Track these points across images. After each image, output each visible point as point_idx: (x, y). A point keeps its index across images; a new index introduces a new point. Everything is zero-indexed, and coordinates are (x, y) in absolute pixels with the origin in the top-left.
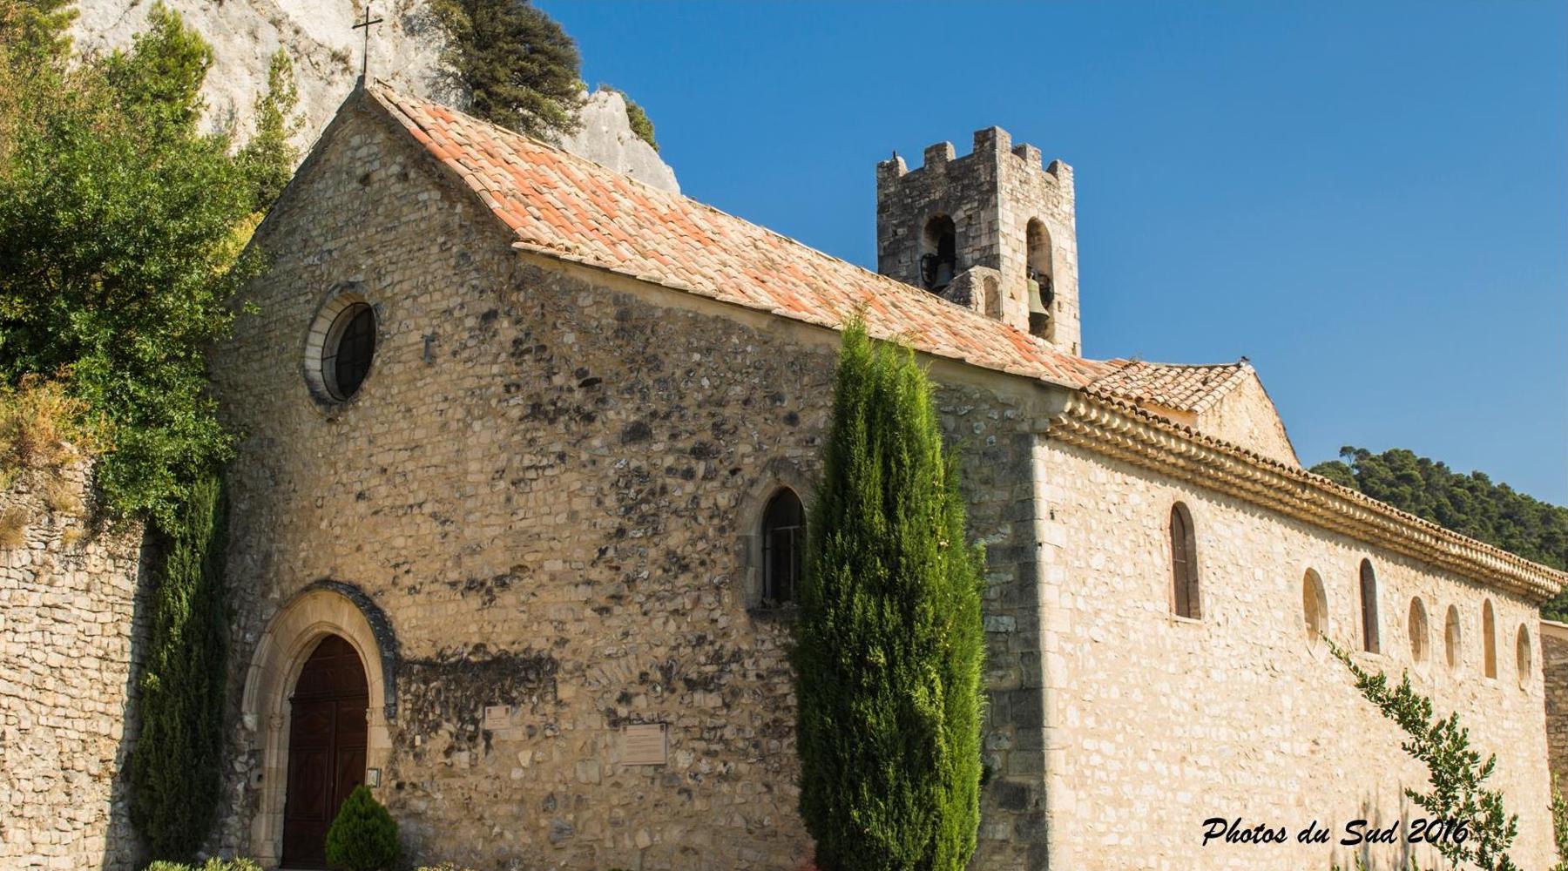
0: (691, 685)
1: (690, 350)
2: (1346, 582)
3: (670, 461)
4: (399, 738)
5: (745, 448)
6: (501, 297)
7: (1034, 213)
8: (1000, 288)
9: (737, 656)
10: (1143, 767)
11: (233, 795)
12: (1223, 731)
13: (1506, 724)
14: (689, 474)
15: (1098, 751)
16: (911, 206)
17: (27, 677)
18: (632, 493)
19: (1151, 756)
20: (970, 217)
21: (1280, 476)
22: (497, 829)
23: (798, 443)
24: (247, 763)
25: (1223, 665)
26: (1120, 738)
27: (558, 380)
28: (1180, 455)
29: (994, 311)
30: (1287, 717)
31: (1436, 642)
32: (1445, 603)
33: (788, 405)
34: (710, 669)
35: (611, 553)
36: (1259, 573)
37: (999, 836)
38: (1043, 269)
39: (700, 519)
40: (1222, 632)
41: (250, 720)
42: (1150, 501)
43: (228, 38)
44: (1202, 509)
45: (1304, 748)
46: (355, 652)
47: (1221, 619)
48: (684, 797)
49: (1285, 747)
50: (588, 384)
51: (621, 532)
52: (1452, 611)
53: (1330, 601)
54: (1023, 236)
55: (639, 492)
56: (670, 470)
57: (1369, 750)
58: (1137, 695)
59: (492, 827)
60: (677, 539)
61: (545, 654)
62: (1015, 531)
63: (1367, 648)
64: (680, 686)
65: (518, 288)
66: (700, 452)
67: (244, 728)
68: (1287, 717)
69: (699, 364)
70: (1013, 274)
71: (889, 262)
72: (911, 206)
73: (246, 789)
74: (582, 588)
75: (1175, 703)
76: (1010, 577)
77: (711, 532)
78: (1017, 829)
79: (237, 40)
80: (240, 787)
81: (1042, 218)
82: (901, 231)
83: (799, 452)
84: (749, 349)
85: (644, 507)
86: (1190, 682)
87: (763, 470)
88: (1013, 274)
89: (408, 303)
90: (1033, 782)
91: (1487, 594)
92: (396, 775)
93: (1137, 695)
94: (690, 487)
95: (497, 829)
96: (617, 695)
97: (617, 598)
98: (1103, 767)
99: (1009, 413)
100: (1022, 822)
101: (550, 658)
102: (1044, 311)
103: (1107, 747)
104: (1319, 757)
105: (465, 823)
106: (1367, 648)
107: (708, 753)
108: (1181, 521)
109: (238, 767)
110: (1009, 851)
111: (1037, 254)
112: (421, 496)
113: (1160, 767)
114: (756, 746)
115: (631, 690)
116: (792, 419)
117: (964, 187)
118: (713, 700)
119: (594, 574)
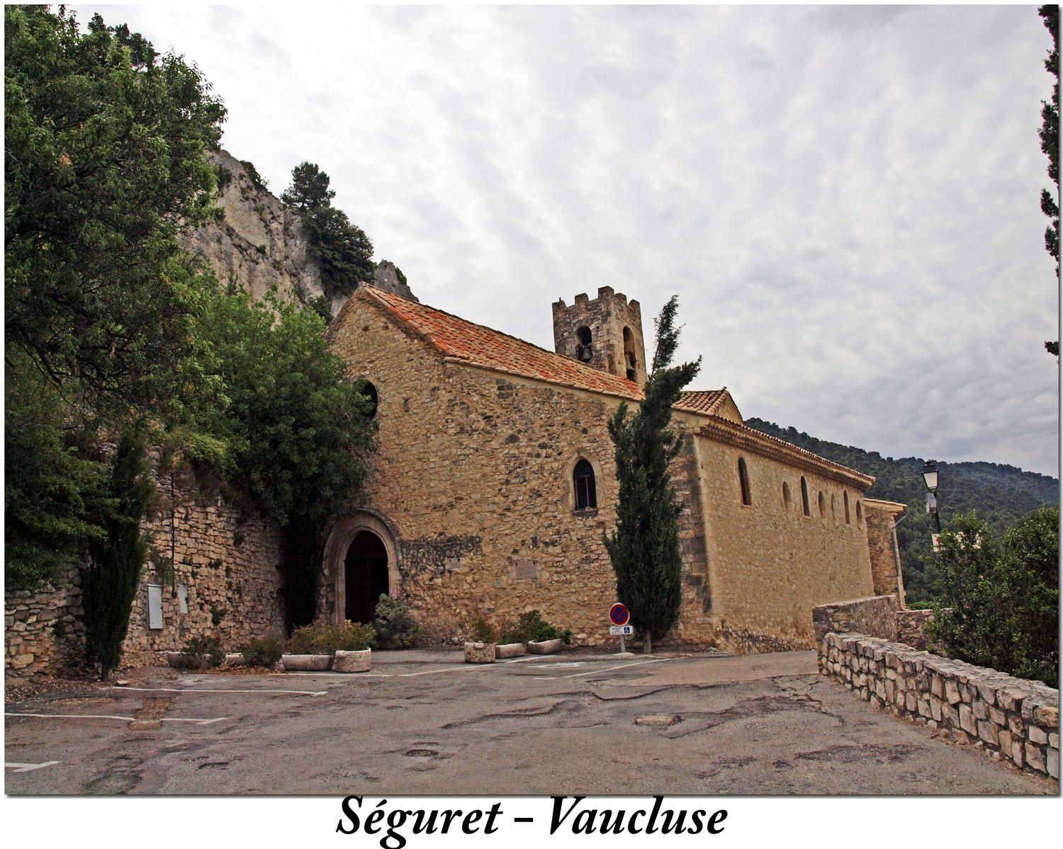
0: (547, 544)
1: (535, 402)
2: (797, 487)
3: (529, 450)
4: (405, 575)
5: (564, 444)
6: (440, 380)
7: (625, 324)
8: (614, 359)
9: (567, 531)
10: (738, 567)
11: (321, 605)
12: (762, 551)
13: (855, 543)
14: (538, 456)
15: (724, 561)
16: (570, 323)
17: (245, 557)
18: (512, 465)
19: (740, 562)
20: (598, 327)
21: (776, 445)
22: (458, 611)
23: (588, 441)
24: (326, 590)
25: (760, 524)
26: (730, 555)
27: (473, 416)
28: (743, 439)
29: (612, 371)
30: (782, 544)
31: (828, 510)
32: (830, 493)
33: (582, 425)
34: (555, 537)
35: (503, 491)
36: (768, 485)
37: (690, 597)
38: (630, 349)
39: (545, 474)
40: (758, 510)
41: (326, 572)
42: (731, 456)
43: (208, 244)
44: (749, 459)
45: (788, 557)
46: (379, 539)
47: (757, 505)
48: (546, 591)
49: (782, 556)
50: (487, 418)
51: (507, 482)
52: (833, 497)
53: (792, 495)
54: (622, 335)
55: (515, 464)
56: (529, 454)
57: (808, 556)
58: (734, 538)
59: (455, 610)
60: (534, 484)
61: (474, 535)
62: (689, 475)
63: (805, 514)
64: (541, 545)
65: (449, 377)
66: (543, 446)
67: (324, 575)
68: (782, 544)
69: (540, 409)
70: (619, 353)
71: (561, 349)
72: (570, 323)
73: (327, 602)
74: (491, 505)
75: (746, 540)
76: (688, 493)
77: (551, 479)
78: (697, 594)
79: (212, 244)
80: (324, 601)
81: (629, 326)
82: (565, 334)
83: (589, 445)
84: (563, 401)
85: (518, 470)
86: (750, 531)
87: (573, 453)
88: (619, 353)
89: (393, 384)
90: (703, 574)
91: (845, 488)
92: (405, 591)
93: (734, 538)
94: (539, 461)
95: (458, 611)
96: (512, 550)
97: (508, 509)
98: (725, 567)
99: (682, 426)
100: (700, 591)
101: (478, 537)
102: (632, 368)
103: (726, 559)
104: (792, 561)
105: (442, 609)
106: (805, 514)
107: (556, 572)
108: (742, 466)
109: (322, 593)
110: (695, 602)
111: (627, 343)
112: (407, 469)
113: (743, 566)
114: (579, 568)
115: (518, 548)
116: (585, 431)
117: (595, 314)
118: (558, 550)
119: (496, 499)
